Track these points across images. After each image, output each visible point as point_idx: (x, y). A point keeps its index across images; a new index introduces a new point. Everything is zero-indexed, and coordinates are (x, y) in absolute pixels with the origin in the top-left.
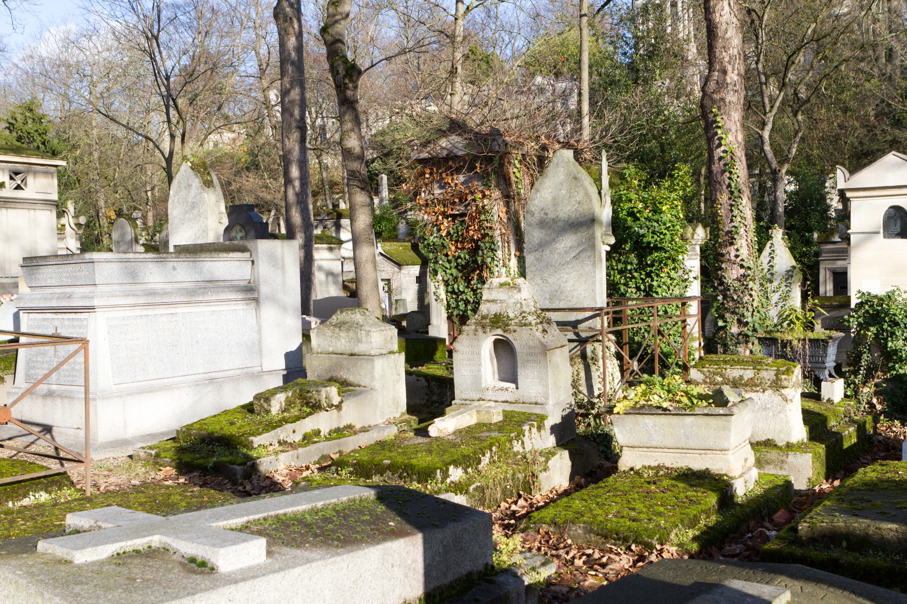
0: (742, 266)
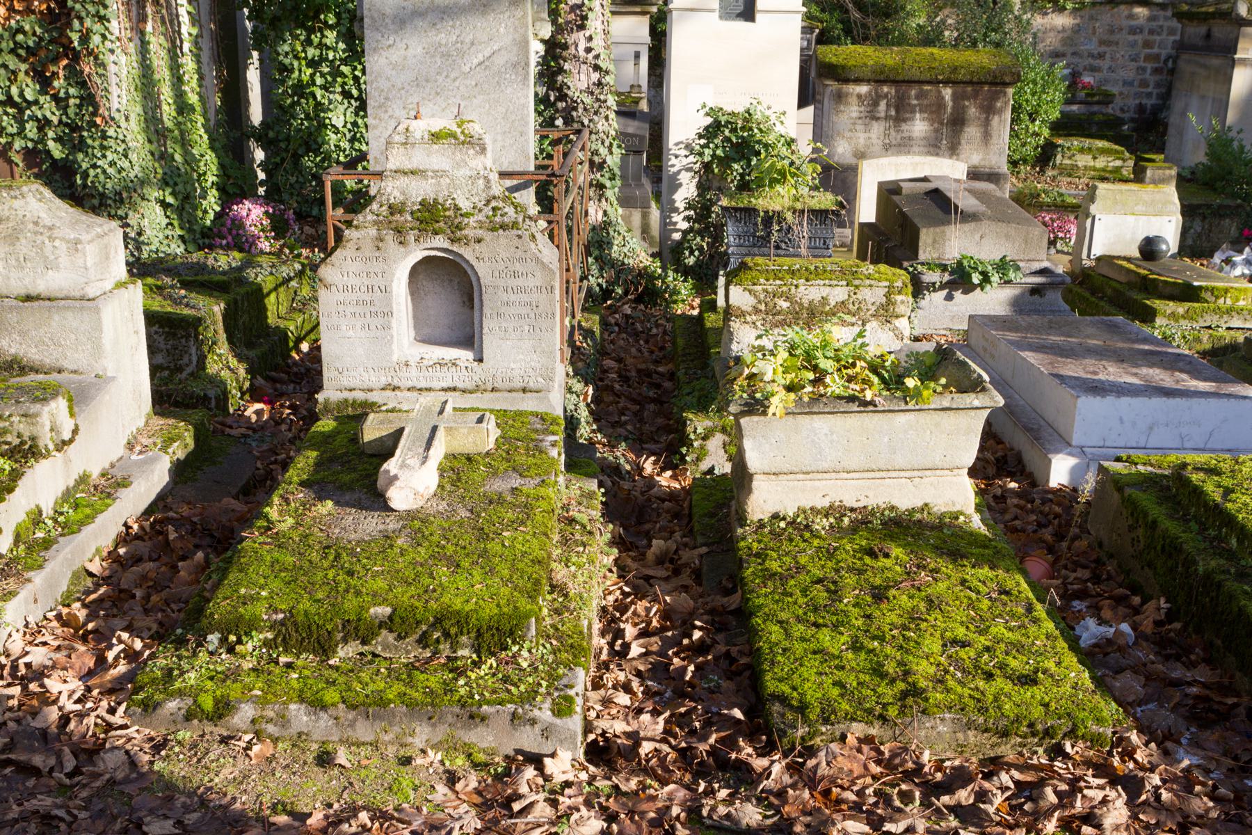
0: (597, 68)
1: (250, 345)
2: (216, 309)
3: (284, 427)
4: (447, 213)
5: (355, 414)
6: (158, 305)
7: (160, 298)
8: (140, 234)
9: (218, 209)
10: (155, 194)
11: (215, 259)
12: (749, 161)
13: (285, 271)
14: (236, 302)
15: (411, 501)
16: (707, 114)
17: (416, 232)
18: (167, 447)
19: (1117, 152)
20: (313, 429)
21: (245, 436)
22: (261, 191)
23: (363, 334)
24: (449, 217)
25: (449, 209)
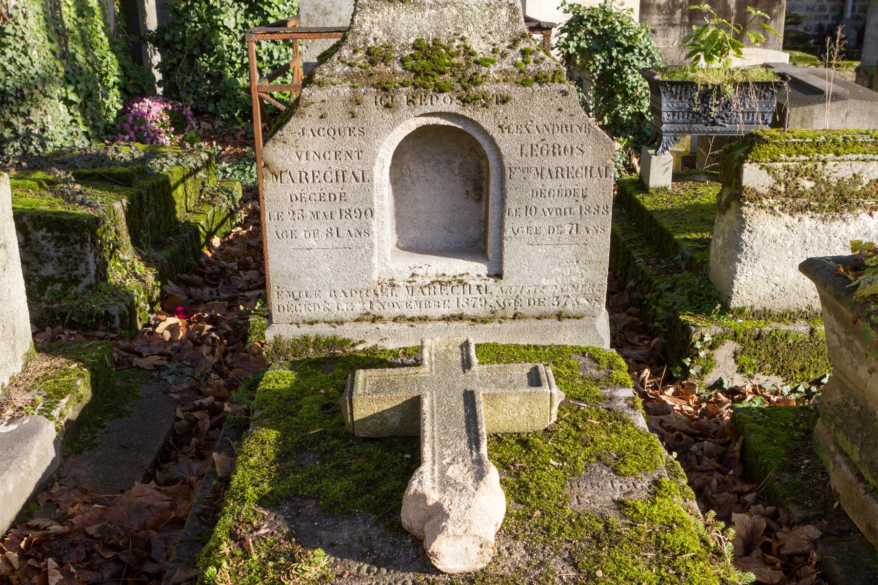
1: (158, 245)
2: (117, 206)
3: (205, 349)
4: (455, 60)
5: (332, 366)
6: (44, 202)
7: (50, 195)
8: (43, 130)
9: (120, 107)
10: (57, 91)
11: (116, 150)
12: (610, 51)
13: (192, 161)
14: (140, 196)
15: (474, 556)
16: (566, 12)
17: (410, 89)
18: (52, 407)
19: (811, 59)
20: (262, 386)
21: (158, 368)
22: (160, 90)
23: (329, 243)
24: (458, 66)
25: (458, 54)
